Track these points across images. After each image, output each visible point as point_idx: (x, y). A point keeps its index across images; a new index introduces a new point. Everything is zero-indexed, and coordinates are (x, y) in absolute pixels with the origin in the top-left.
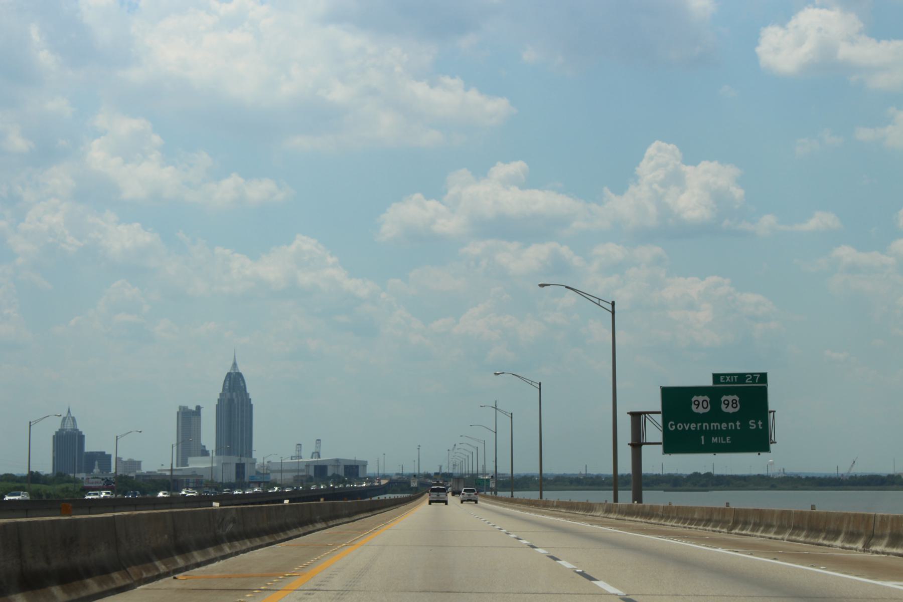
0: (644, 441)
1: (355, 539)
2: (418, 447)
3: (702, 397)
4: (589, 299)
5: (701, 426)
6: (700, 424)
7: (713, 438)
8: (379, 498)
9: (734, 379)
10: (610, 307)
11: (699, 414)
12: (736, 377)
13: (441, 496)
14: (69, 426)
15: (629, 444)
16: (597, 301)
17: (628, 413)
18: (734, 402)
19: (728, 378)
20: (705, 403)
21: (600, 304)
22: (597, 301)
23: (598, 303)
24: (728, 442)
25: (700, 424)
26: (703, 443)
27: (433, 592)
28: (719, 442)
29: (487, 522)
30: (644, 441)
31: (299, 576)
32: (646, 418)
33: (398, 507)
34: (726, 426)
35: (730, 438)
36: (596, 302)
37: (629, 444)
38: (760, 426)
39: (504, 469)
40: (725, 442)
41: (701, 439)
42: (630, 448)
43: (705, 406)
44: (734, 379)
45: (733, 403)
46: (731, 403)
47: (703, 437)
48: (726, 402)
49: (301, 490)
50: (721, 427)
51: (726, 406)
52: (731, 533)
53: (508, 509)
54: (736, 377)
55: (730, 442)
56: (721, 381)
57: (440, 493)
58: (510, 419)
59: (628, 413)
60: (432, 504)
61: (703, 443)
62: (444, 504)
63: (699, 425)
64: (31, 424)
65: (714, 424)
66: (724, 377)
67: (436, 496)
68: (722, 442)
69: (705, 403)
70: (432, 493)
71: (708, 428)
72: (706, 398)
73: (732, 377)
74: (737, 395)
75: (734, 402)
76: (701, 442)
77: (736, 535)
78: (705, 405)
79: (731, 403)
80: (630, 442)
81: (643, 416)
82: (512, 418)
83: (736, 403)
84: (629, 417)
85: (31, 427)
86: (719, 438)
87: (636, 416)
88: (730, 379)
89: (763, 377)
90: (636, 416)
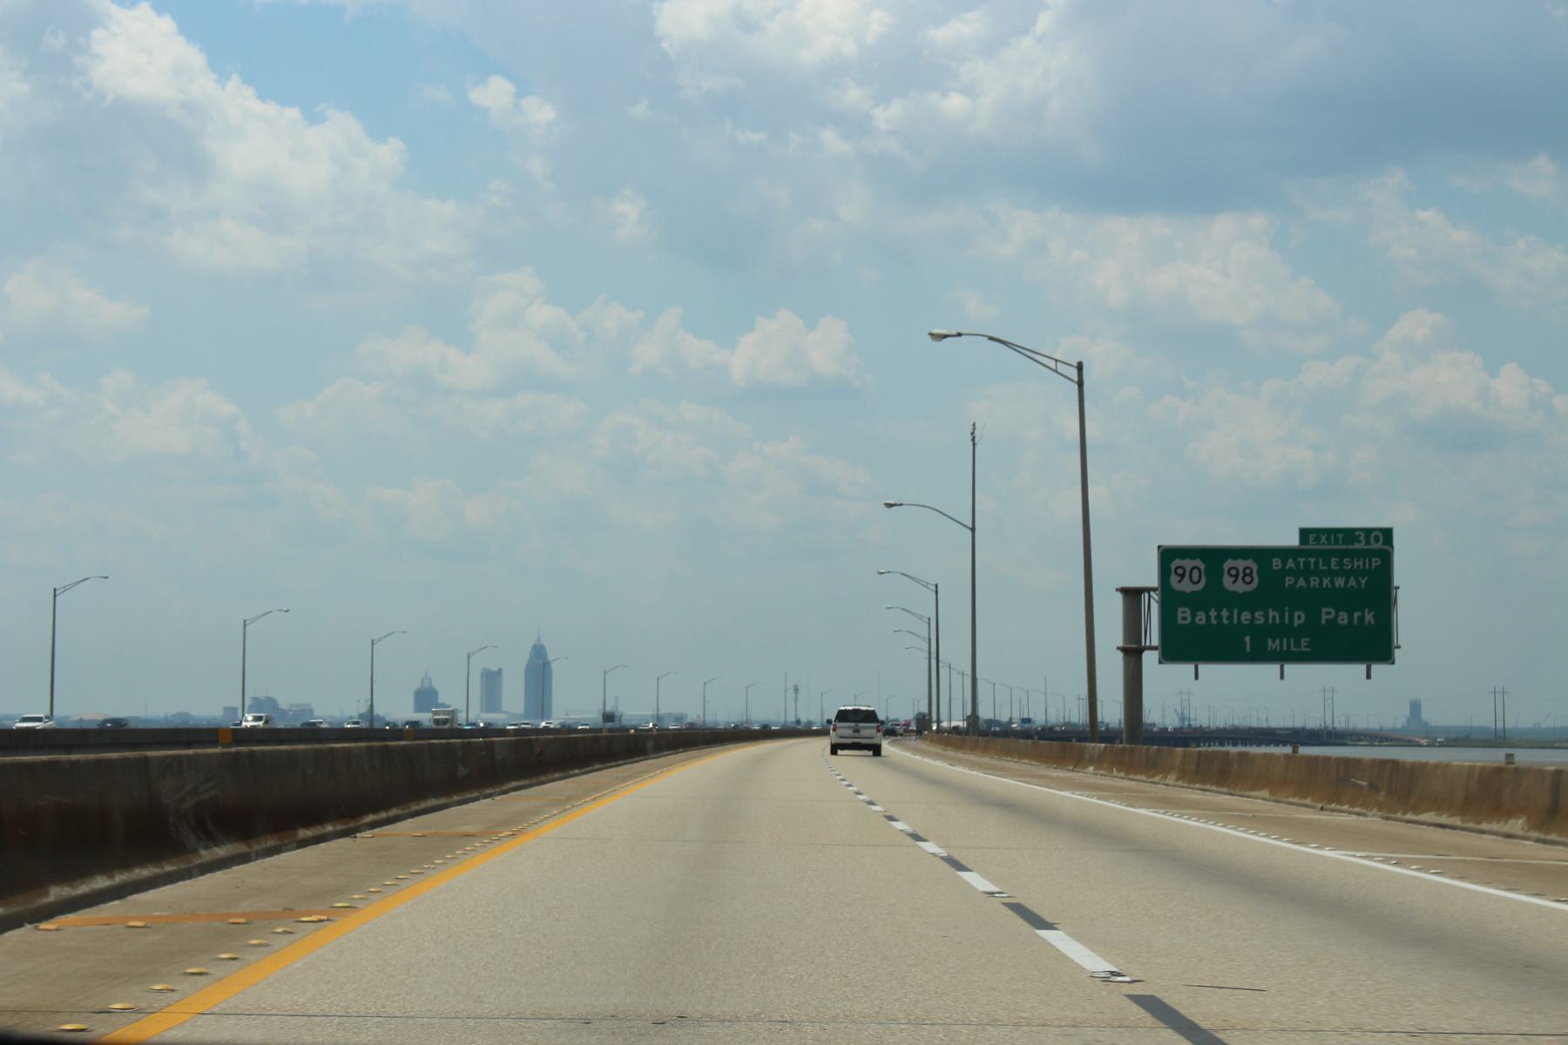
0: (1148, 644)
1: (83, 889)
3: (1192, 561)
4: (1029, 357)
7: (1270, 641)
8: (856, 731)
10: (1074, 374)
11: (1236, 593)
12: (1340, 536)
13: (864, 733)
14: (426, 685)
15: (1118, 648)
16: (1052, 364)
17: (1117, 590)
19: (1323, 538)
20: (1196, 573)
21: (1059, 370)
22: (1052, 364)
23: (1054, 367)
24: (1303, 649)
25: (1359, 614)
26: (1248, 650)
28: (1285, 648)
29: (854, 789)
30: (1148, 644)
31: (328, 920)
32: (1152, 600)
33: (620, 765)
34: (1249, 616)
35: (1308, 639)
36: (1050, 366)
37: (1118, 648)
38: (1213, 619)
39: (512, 711)
40: (1298, 649)
41: (1245, 643)
42: (1120, 655)
43: (1195, 578)
45: (1245, 575)
46: (1241, 575)
47: (1247, 639)
48: (1233, 572)
49: (408, 730)
51: (1233, 579)
53: (939, 763)
55: (1308, 649)
57: (861, 725)
58: (934, 594)
59: (1117, 590)
60: (839, 752)
61: (1248, 650)
62: (871, 753)
63: (1357, 614)
64: (57, 592)
65: (1179, 618)
66: (1315, 535)
67: (849, 732)
68: (1293, 649)
69: (1196, 573)
70: (839, 724)
71: (1277, 621)
73: (1332, 536)
74: (1201, 560)
75: (1248, 571)
76: (1245, 648)
79: (1241, 575)
80: (1121, 644)
81: (1147, 595)
82: (937, 592)
83: (1251, 575)
84: (1120, 596)
85: (57, 598)
86: (1285, 640)
87: (1132, 596)
89: (1387, 534)
90: (1132, 596)
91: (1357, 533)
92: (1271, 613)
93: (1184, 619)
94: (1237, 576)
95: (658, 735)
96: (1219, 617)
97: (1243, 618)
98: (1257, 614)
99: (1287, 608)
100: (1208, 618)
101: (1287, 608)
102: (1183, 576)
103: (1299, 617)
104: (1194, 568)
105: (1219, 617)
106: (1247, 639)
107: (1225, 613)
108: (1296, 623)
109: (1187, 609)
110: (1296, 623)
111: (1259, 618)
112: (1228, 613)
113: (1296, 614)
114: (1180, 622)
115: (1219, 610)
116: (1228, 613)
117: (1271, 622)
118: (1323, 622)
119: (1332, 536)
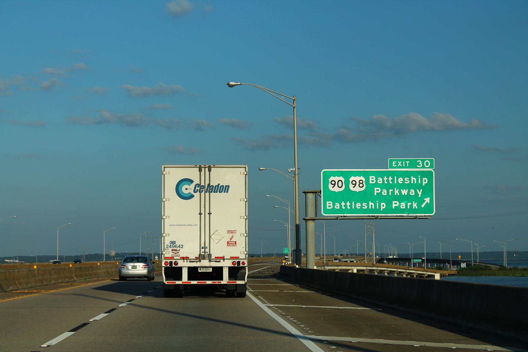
2: (169, 173)
5: (393, 192)
6: (392, 190)
9: (406, 164)
18: (361, 182)
19: (400, 163)
20: (340, 183)
25: (392, 190)
27: (174, 225)
34: (360, 205)
38: (348, 206)
43: (340, 185)
44: (406, 164)
45: (360, 183)
46: (358, 183)
47: (236, 295)
48: (333, 183)
50: (355, 206)
52: (232, 258)
54: (408, 162)
56: (394, 166)
65: (393, 165)
69: (340, 183)
72: (341, 178)
73: (404, 162)
75: (361, 182)
77: (288, 287)
78: (340, 185)
83: (362, 183)
88: (402, 164)
91: (418, 161)
92: (370, 204)
93: (372, 181)
94: (355, 184)
95: (120, 254)
96: (388, 181)
97: (357, 205)
98: (406, 179)
99: (419, 176)
100: (383, 181)
101: (377, 202)
102: (335, 184)
103: (425, 181)
104: (339, 181)
105: (346, 206)
106: (236, 295)
107: (348, 204)
108: (424, 183)
109: (331, 202)
110: (424, 183)
111: (407, 180)
112: (392, 179)
113: (424, 179)
114: (371, 182)
115: (346, 203)
116: (392, 179)
117: (370, 208)
118: (393, 208)
119: (404, 162)
